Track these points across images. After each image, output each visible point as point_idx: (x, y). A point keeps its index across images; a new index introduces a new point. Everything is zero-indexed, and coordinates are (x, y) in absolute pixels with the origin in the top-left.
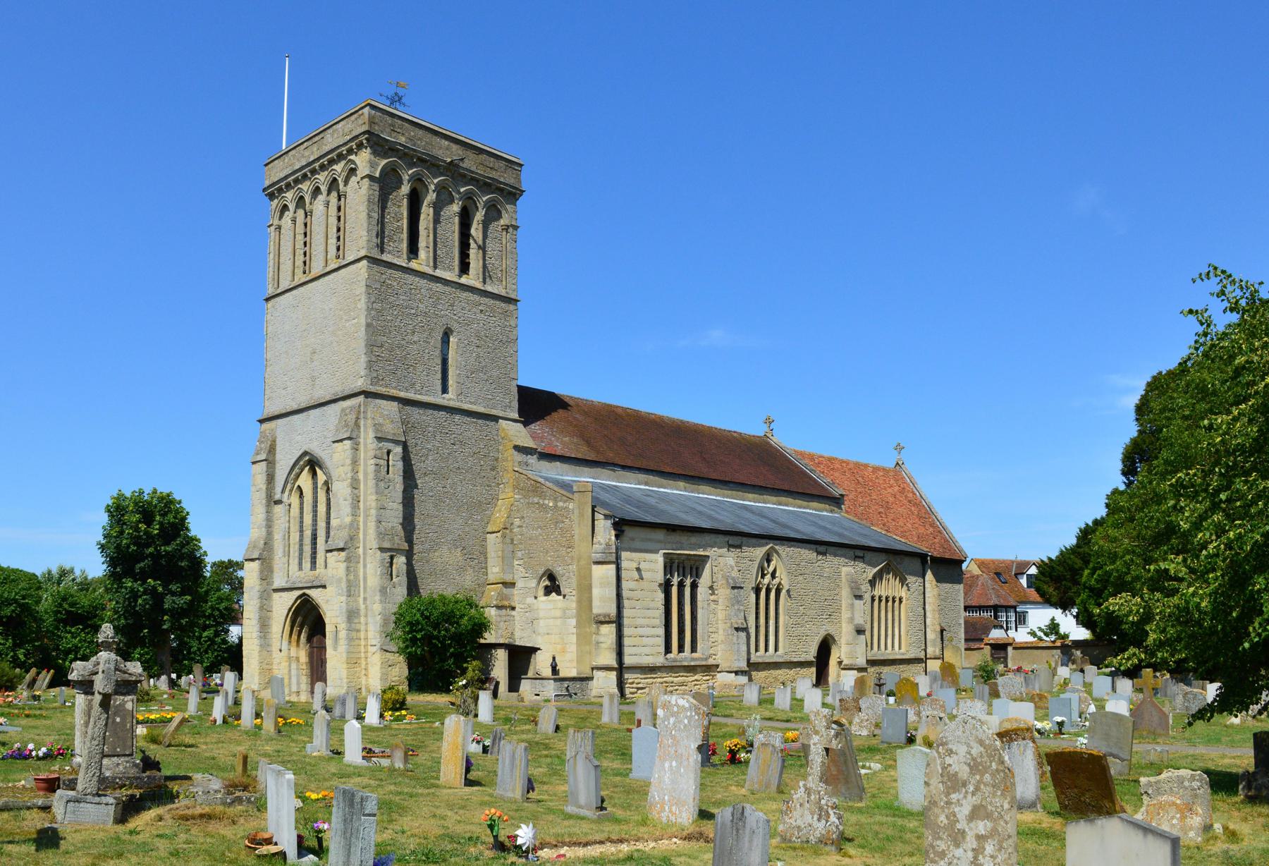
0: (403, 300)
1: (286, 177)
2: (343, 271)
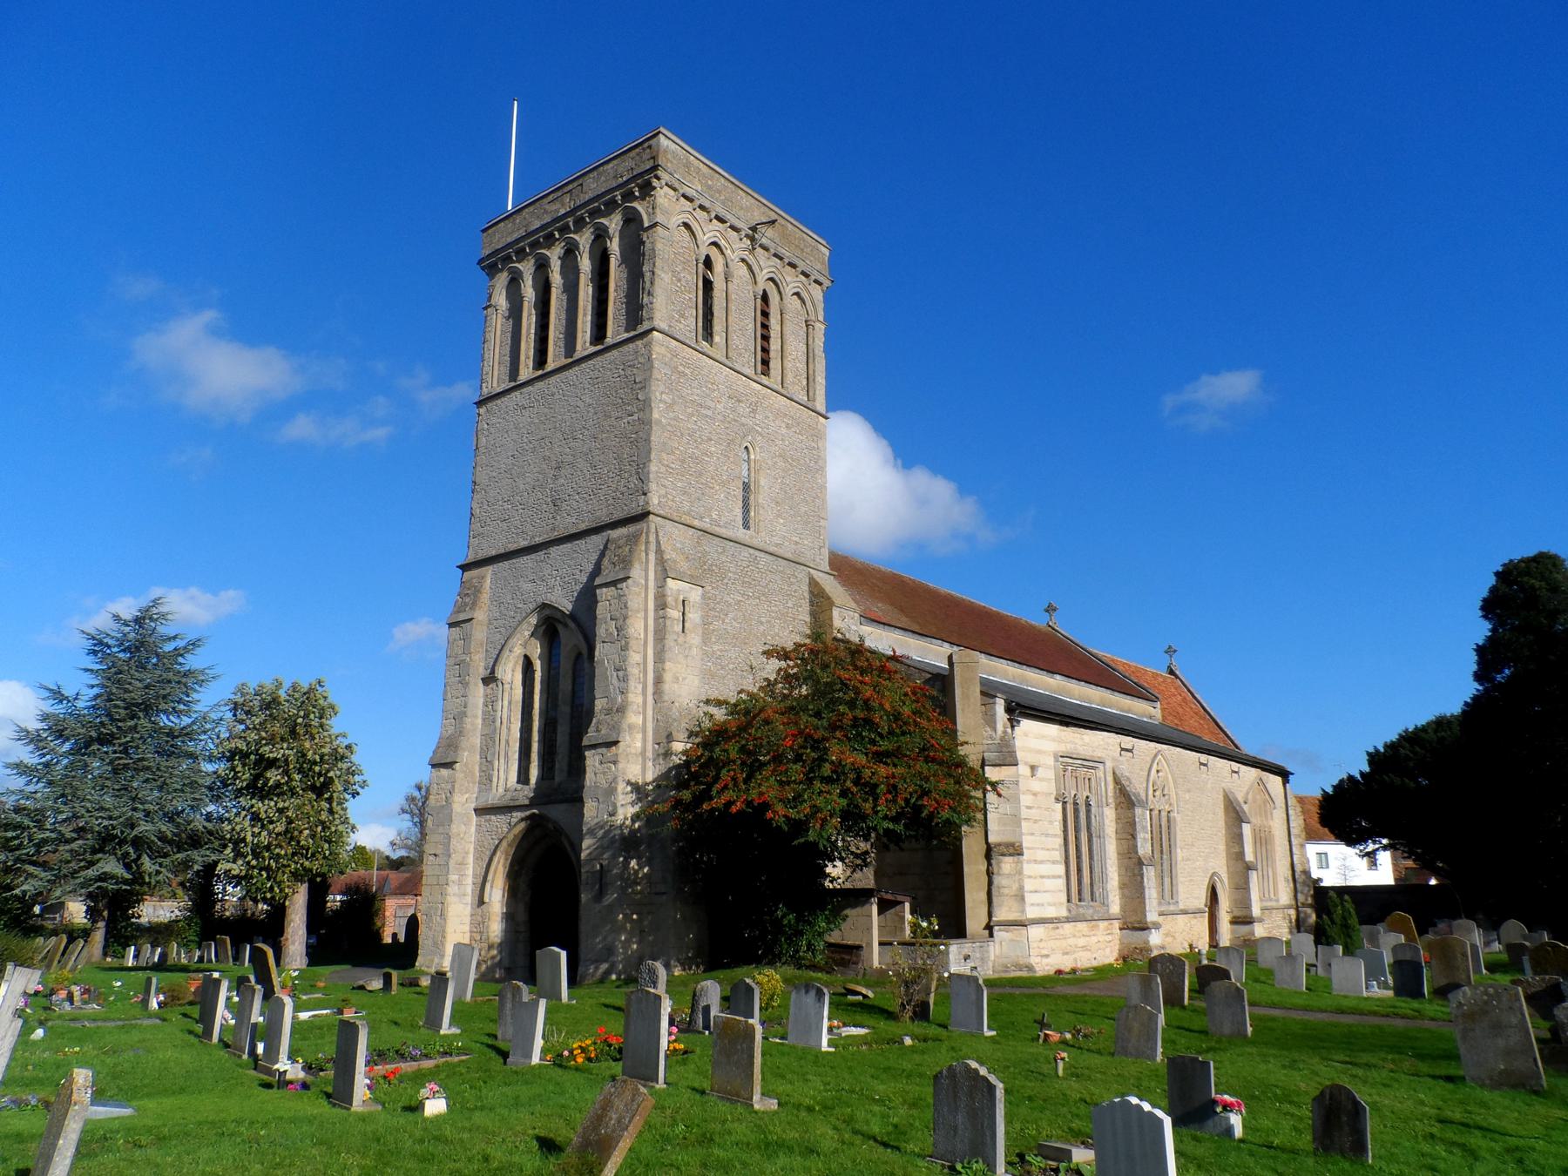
0: (698, 395)
1: (517, 241)
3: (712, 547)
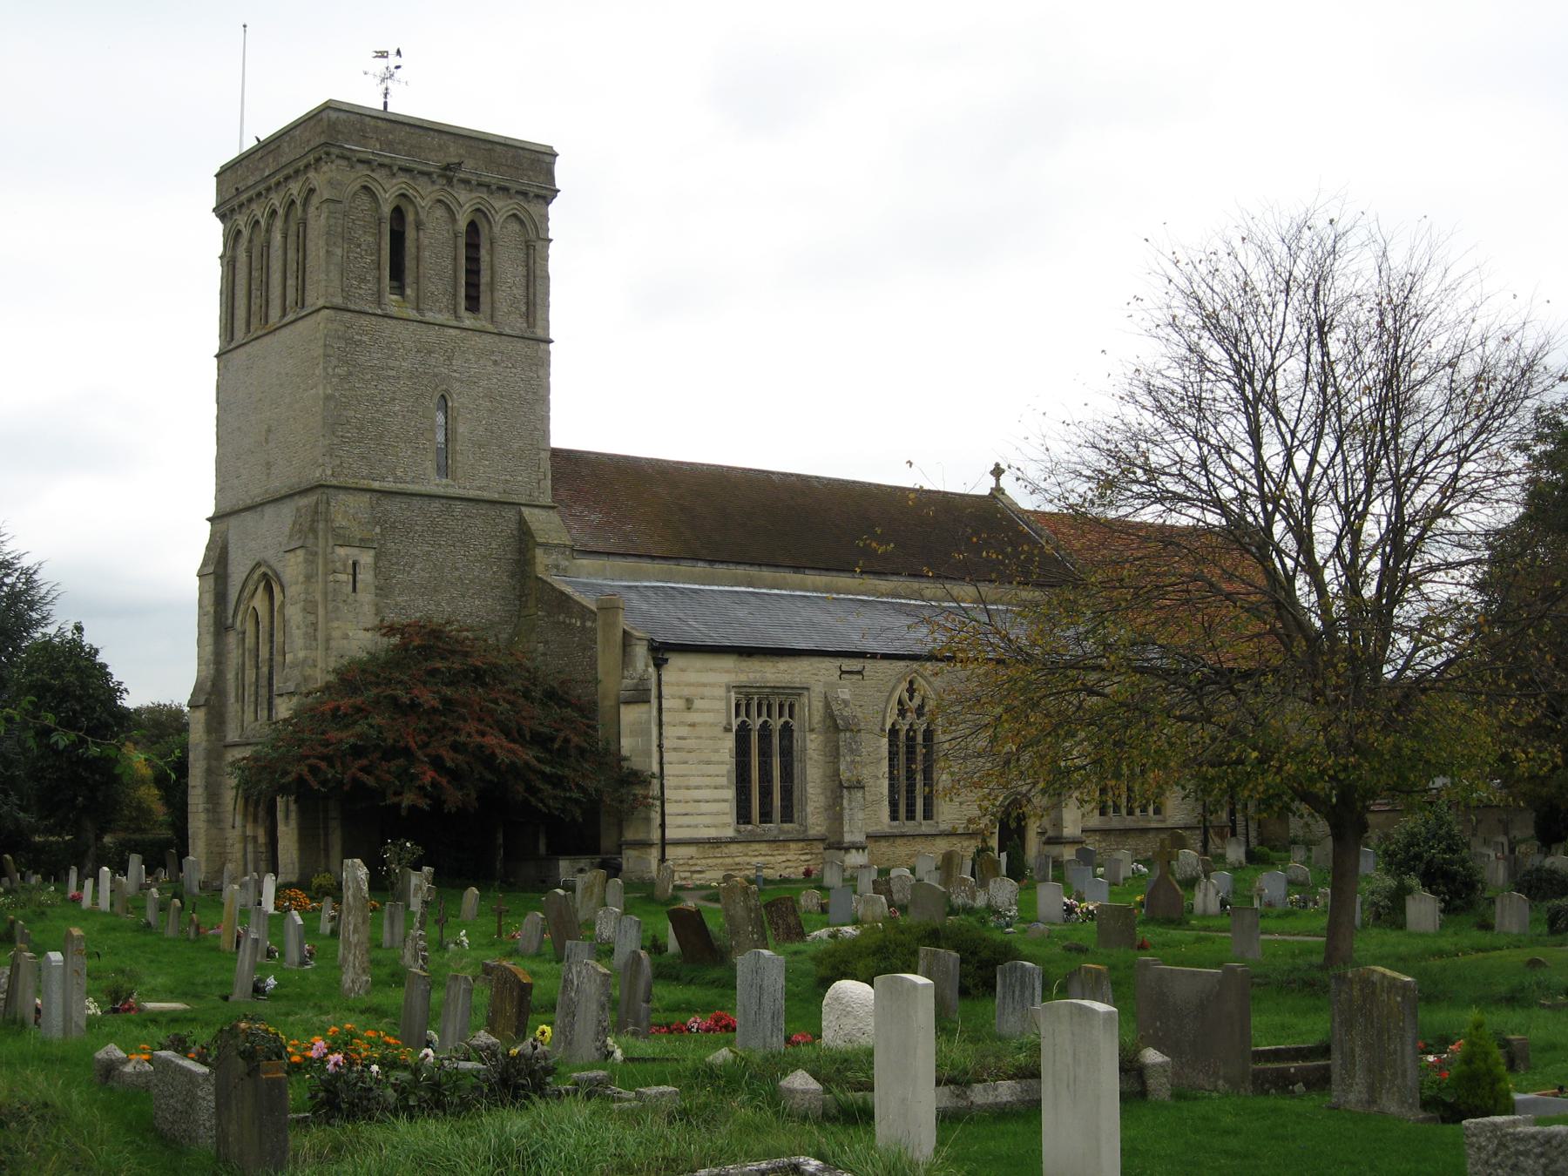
2: (300, 323)
3: (394, 507)
